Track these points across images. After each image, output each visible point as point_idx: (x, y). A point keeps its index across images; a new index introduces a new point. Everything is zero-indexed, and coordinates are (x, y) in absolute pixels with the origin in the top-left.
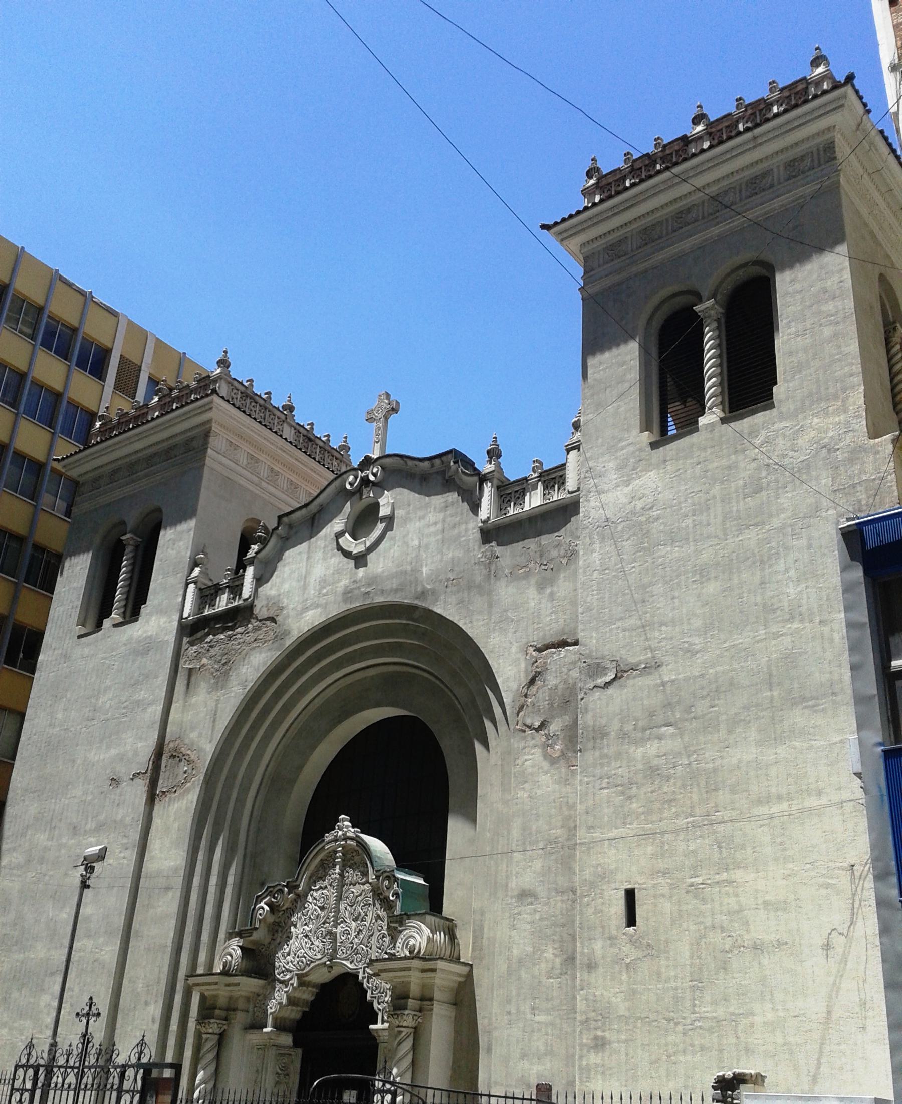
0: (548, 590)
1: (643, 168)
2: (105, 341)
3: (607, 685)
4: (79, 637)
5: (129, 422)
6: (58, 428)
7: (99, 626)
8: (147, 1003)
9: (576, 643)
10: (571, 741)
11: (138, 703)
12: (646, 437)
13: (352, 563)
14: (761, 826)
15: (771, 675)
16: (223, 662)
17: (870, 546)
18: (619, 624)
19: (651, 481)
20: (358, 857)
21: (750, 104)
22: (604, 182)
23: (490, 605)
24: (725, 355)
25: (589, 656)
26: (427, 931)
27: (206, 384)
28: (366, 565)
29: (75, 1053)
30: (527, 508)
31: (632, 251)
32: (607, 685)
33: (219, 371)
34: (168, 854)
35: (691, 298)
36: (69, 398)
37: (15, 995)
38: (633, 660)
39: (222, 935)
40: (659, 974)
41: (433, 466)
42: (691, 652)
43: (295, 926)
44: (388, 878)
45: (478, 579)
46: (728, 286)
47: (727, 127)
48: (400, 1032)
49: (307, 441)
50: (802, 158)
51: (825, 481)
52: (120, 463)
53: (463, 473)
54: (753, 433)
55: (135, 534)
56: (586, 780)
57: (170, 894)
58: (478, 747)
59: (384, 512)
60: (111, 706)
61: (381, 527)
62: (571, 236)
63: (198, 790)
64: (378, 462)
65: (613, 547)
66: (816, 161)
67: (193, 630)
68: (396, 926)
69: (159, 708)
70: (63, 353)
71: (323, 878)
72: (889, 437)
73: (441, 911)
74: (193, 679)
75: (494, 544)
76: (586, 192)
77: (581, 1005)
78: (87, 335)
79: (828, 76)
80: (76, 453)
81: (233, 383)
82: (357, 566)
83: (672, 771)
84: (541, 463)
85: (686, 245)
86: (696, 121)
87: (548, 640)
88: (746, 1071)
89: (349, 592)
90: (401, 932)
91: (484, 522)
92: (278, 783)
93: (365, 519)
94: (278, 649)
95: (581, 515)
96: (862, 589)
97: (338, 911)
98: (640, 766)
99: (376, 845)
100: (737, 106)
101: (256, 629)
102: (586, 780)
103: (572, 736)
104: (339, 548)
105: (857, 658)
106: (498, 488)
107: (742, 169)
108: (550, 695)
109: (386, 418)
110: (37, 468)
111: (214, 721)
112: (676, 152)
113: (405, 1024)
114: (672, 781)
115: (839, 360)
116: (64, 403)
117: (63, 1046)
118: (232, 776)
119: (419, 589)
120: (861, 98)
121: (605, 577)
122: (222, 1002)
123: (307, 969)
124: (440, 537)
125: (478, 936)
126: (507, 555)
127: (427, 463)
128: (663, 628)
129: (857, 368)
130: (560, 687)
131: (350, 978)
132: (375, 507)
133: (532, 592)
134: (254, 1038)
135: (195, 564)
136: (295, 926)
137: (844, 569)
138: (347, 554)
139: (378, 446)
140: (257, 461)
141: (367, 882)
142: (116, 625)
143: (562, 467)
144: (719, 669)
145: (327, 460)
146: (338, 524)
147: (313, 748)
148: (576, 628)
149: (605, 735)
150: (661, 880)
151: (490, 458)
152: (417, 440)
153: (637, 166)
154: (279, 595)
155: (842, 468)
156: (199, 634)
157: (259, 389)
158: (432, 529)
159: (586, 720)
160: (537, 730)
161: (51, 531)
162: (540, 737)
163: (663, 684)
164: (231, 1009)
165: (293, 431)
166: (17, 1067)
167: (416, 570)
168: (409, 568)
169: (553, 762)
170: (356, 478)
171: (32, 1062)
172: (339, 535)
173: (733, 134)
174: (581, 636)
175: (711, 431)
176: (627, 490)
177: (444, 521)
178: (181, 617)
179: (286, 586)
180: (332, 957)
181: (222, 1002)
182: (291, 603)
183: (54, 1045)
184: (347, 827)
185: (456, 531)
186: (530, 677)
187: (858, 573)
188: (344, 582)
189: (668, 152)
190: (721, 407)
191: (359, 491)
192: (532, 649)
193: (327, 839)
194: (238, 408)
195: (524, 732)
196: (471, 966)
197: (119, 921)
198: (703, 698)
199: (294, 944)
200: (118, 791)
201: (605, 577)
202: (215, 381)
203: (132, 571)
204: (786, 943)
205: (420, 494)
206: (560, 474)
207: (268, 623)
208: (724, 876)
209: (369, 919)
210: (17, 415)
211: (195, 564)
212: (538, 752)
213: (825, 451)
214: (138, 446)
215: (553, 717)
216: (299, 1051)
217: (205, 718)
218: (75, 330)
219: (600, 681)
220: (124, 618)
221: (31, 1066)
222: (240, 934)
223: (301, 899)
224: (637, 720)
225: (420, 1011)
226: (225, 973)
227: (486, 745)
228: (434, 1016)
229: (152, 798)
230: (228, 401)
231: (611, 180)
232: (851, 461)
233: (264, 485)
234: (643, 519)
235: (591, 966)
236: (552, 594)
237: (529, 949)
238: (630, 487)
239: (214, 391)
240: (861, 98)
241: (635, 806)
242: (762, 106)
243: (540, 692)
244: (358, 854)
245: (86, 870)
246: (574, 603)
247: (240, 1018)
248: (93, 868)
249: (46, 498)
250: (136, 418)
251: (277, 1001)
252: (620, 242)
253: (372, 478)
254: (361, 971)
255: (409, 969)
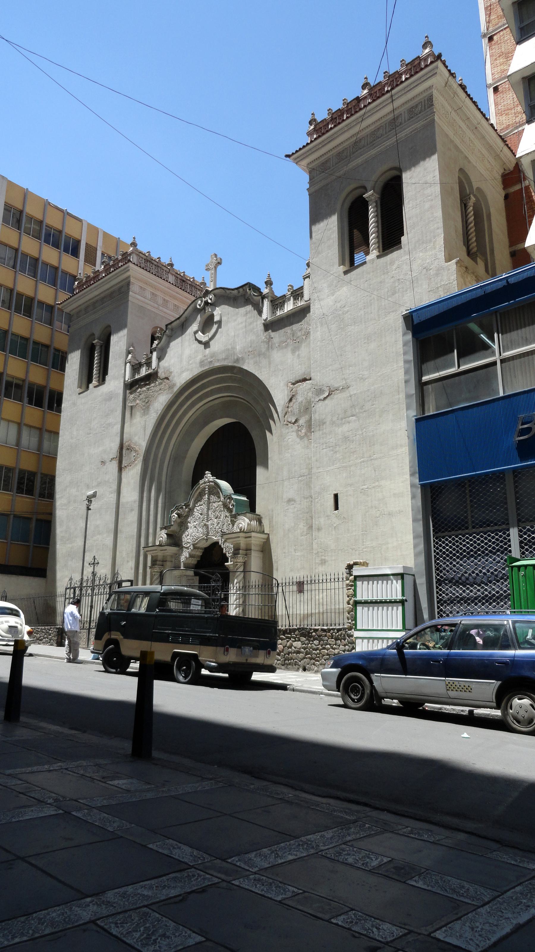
0: (297, 353)
1: (337, 117)
2: (76, 236)
3: (325, 398)
4: (79, 394)
5: (91, 280)
6: (59, 286)
7: (88, 387)
8: (128, 562)
9: (310, 379)
10: (309, 428)
11: (109, 424)
12: (342, 269)
13: (203, 346)
14: (393, 460)
15: (399, 387)
16: (146, 401)
17: (415, 323)
18: (330, 368)
19: (344, 291)
20: (215, 490)
21: (409, 64)
22: (318, 127)
23: (270, 364)
24: (380, 221)
25: (316, 385)
26: (247, 520)
27: (126, 257)
28: (209, 347)
29: (90, 580)
30: (286, 311)
31: (333, 166)
32: (325, 398)
33: (131, 249)
34: (130, 494)
35: (362, 190)
36: (62, 269)
37: (70, 563)
38: (336, 385)
39: (158, 529)
40: (348, 530)
41: (239, 292)
42: (363, 379)
43: (190, 523)
44: (229, 498)
45: (263, 350)
46: (380, 185)
47: (379, 90)
48: (237, 565)
49: (183, 282)
50: (417, 106)
51: (425, 286)
52: (88, 303)
53: (254, 295)
54: (392, 263)
55: (100, 340)
56: (316, 445)
57: (133, 512)
58: (268, 434)
59: (216, 319)
60: (97, 427)
61: (215, 327)
62: (302, 160)
63: (141, 464)
64: (213, 292)
65: (327, 328)
66: (423, 108)
67: (131, 386)
68: (234, 518)
69: (119, 426)
70: (56, 245)
71: (200, 501)
72: (454, 261)
73: (255, 512)
74: (133, 411)
75: (270, 331)
76: (309, 134)
77: (315, 546)
78: (67, 234)
79: (431, 54)
80: (69, 298)
81: (139, 254)
82: (205, 348)
83: (355, 438)
84: (292, 286)
85: (360, 160)
86: (364, 87)
87: (298, 378)
88: (358, 561)
89: (202, 362)
90: (236, 522)
91: (265, 320)
92: (178, 459)
93: (208, 323)
94: (171, 393)
95: (311, 313)
96: (411, 344)
97: (208, 515)
98: (340, 437)
99: (224, 484)
100: (384, 77)
101: (160, 384)
102: (316, 445)
103: (309, 425)
104: (196, 339)
105: (407, 377)
106: (271, 301)
107: (386, 115)
108: (299, 406)
109: (216, 268)
110: (51, 308)
111: (145, 431)
112: (354, 107)
113: (239, 561)
114: (354, 442)
115: (432, 221)
116: (60, 273)
117: (85, 578)
118: (156, 455)
119: (236, 358)
120: (447, 67)
121: (323, 344)
122: (160, 558)
123: (197, 541)
124: (244, 330)
125: (271, 522)
126: (277, 336)
127: (236, 291)
128: (351, 368)
129: (441, 224)
130: (304, 402)
131: (216, 544)
132: (212, 316)
133: (289, 355)
134: (176, 573)
135: (129, 352)
136: (190, 523)
137: (404, 334)
138: (200, 342)
139: (212, 283)
140: (156, 295)
141: (220, 501)
142: (95, 387)
143: (302, 288)
144: (376, 386)
145: (194, 291)
146: (195, 327)
147: (193, 440)
148: (310, 371)
149: (324, 423)
150: (349, 488)
151: (267, 285)
152: (230, 280)
153: (334, 116)
154: (169, 366)
155: (433, 279)
156: (134, 388)
157: (154, 256)
158: (241, 326)
159: (315, 417)
160: (294, 423)
161: (61, 341)
162: (295, 427)
163: (351, 396)
164: (164, 561)
165: (174, 277)
166: (66, 589)
167: (234, 348)
168: (230, 347)
169: (301, 438)
170: (202, 301)
171: (72, 586)
172: (196, 332)
173: (399, 83)
174: (313, 375)
175: (373, 263)
176: (332, 298)
177: (246, 321)
178: (125, 381)
179: (172, 361)
180: (208, 534)
181: (160, 558)
182: (175, 370)
183: (82, 579)
184: (209, 476)
185: (252, 326)
186: (290, 398)
187: (409, 336)
188: (200, 357)
189: (350, 107)
190: (377, 250)
191: (204, 309)
192: (290, 384)
193: (201, 483)
194: (143, 268)
195: (288, 425)
196: (269, 534)
197: (112, 526)
198: (369, 401)
199: (190, 531)
200: (105, 467)
201: (323, 344)
202: (130, 255)
203: (100, 359)
204: (402, 511)
205: (233, 307)
206: (301, 291)
207: (165, 380)
208: (377, 484)
209: (222, 517)
210: (36, 281)
211: (129, 352)
212: (294, 434)
213: (425, 270)
214: (96, 293)
215: (301, 417)
216: (198, 578)
217: (140, 430)
218: (60, 232)
219: (322, 397)
220: (99, 383)
221: (72, 588)
222: (165, 528)
223: (191, 511)
224: (339, 415)
225: (246, 555)
226: (160, 545)
227: (272, 433)
228: (252, 557)
229: (120, 469)
230: (137, 265)
231: (321, 126)
232: (437, 275)
233: (161, 308)
234: (340, 312)
235: (319, 529)
236: (299, 355)
237: (293, 525)
238: (334, 296)
239: (129, 261)
240: (447, 67)
241: (338, 456)
242: (397, 76)
243: (294, 405)
244: (215, 489)
245: (88, 502)
246: (309, 359)
247: (169, 565)
248: (91, 501)
249: (57, 323)
250: (94, 278)
251: (185, 555)
252: (327, 161)
253: (209, 301)
254: (220, 540)
255: (239, 537)
